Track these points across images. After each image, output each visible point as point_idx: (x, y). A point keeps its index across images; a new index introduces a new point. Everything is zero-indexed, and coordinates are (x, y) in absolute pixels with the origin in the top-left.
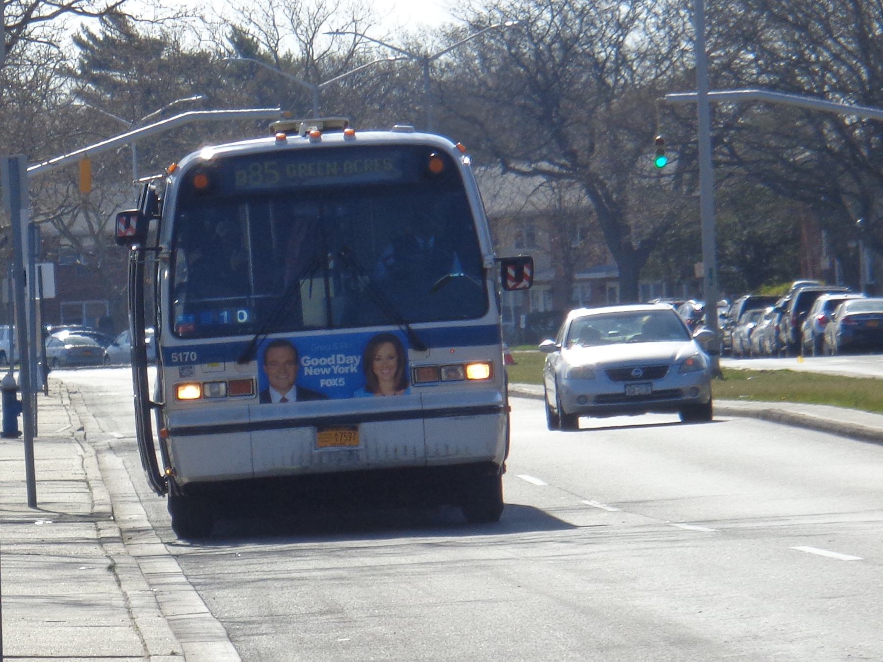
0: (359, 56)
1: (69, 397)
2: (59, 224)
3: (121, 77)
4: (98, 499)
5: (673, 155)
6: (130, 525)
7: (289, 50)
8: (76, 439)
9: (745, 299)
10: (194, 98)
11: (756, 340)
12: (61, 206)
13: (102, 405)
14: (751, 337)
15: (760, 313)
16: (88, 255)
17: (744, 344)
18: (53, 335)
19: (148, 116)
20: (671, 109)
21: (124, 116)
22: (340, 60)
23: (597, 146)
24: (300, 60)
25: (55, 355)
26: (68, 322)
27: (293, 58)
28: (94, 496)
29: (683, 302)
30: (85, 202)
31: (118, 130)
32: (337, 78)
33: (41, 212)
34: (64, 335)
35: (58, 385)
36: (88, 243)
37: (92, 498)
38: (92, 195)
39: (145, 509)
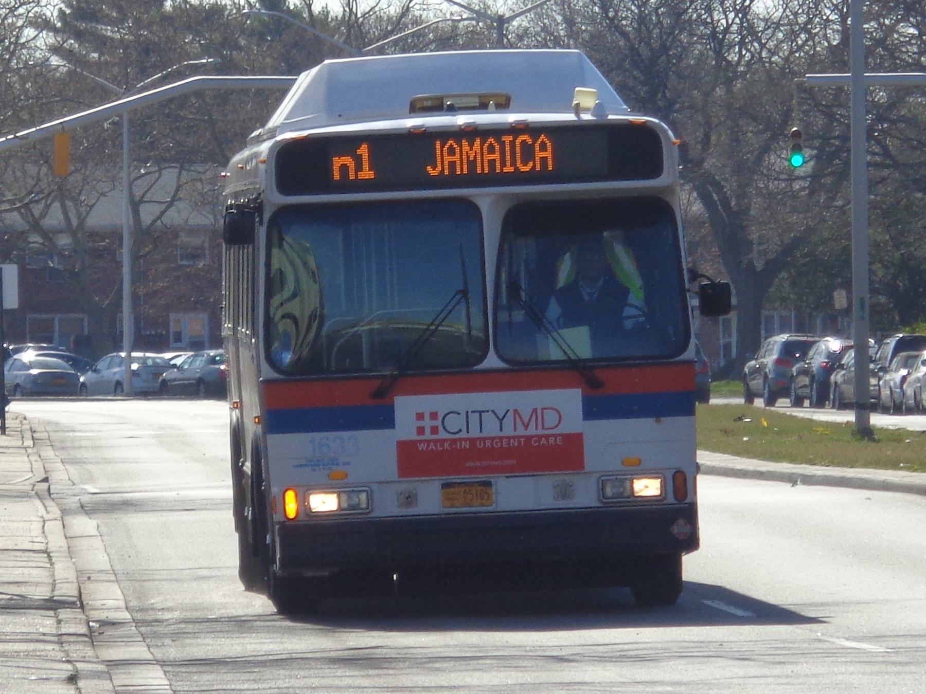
0: (414, 15)
1: (33, 437)
2: (27, 215)
3: (112, 31)
4: (61, 577)
5: (808, 152)
6: (103, 615)
7: (327, 5)
8: (36, 493)
9: (898, 338)
10: (205, 61)
11: (910, 392)
12: (30, 193)
13: (74, 448)
14: (905, 386)
15: (917, 357)
16: (64, 256)
17: (895, 396)
18: (16, 357)
19: (146, 82)
20: (808, 93)
21: (114, 80)
22: (389, 19)
23: (714, 138)
24: (339, 18)
25: (18, 381)
26: (36, 339)
27: (330, 16)
28: (56, 573)
29: (817, 339)
30: (60, 189)
31: (106, 96)
32: (385, 41)
33: (5, 199)
34: (29, 355)
35: (18, 421)
36: (64, 241)
37: (53, 575)
38: (71, 179)
39: (122, 592)
